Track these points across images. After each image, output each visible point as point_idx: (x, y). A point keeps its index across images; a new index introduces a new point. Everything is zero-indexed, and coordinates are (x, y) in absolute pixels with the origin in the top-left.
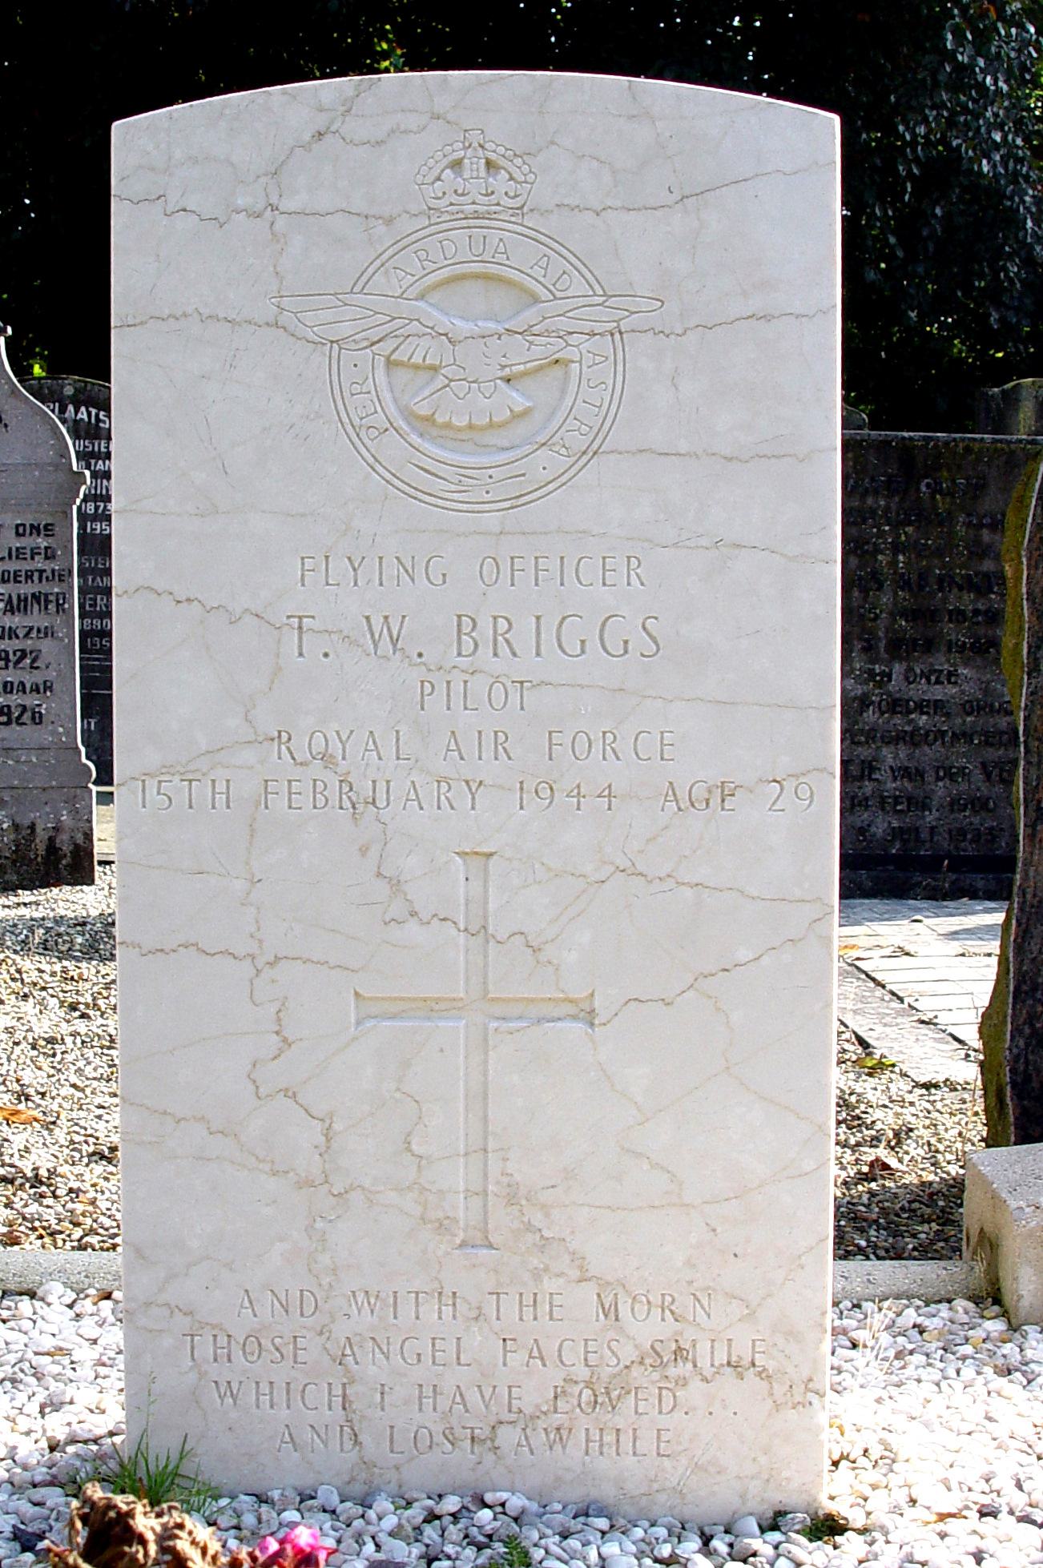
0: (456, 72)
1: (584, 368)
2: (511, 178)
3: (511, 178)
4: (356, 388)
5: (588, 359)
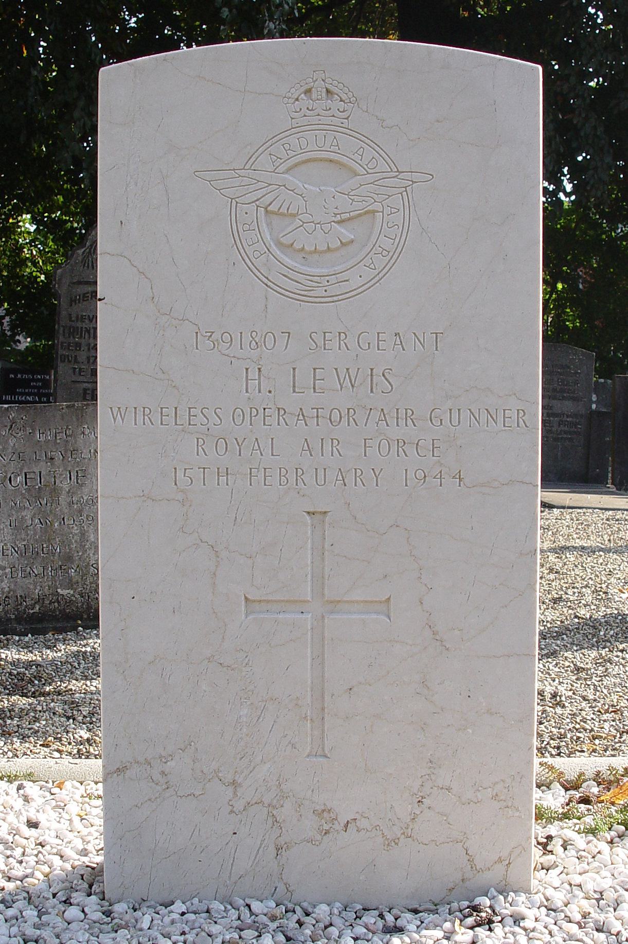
0: (589, 496)
1: (385, 215)
3: (341, 101)
5: (387, 210)
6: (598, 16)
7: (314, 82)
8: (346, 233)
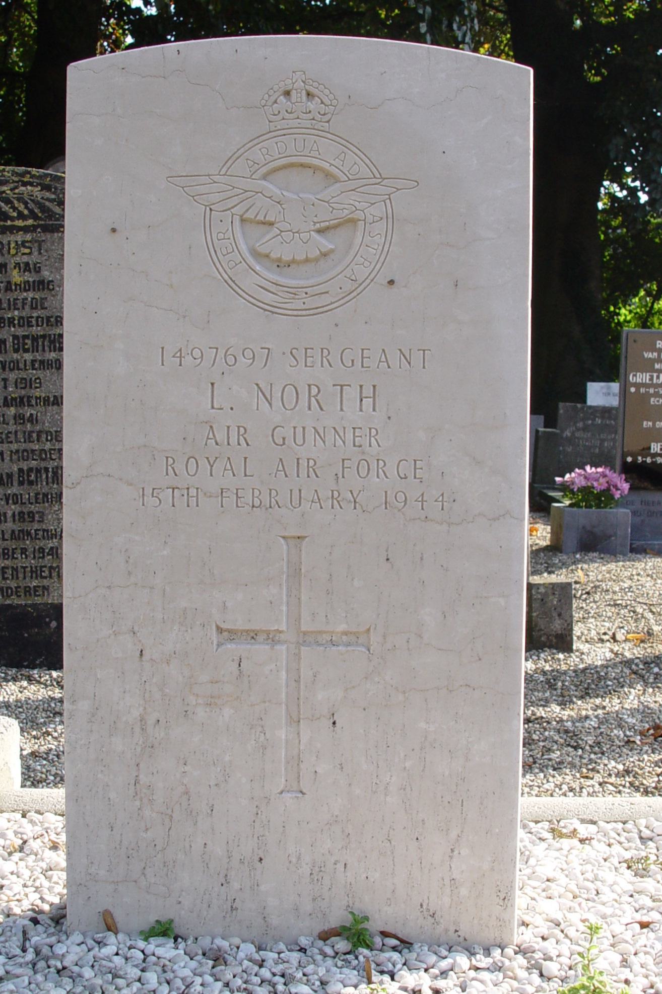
2: (322, 103)
3: (322, 103)
4: (221, 236)
6: (596, 75)
7: (294, 84)
8: (325, 243)
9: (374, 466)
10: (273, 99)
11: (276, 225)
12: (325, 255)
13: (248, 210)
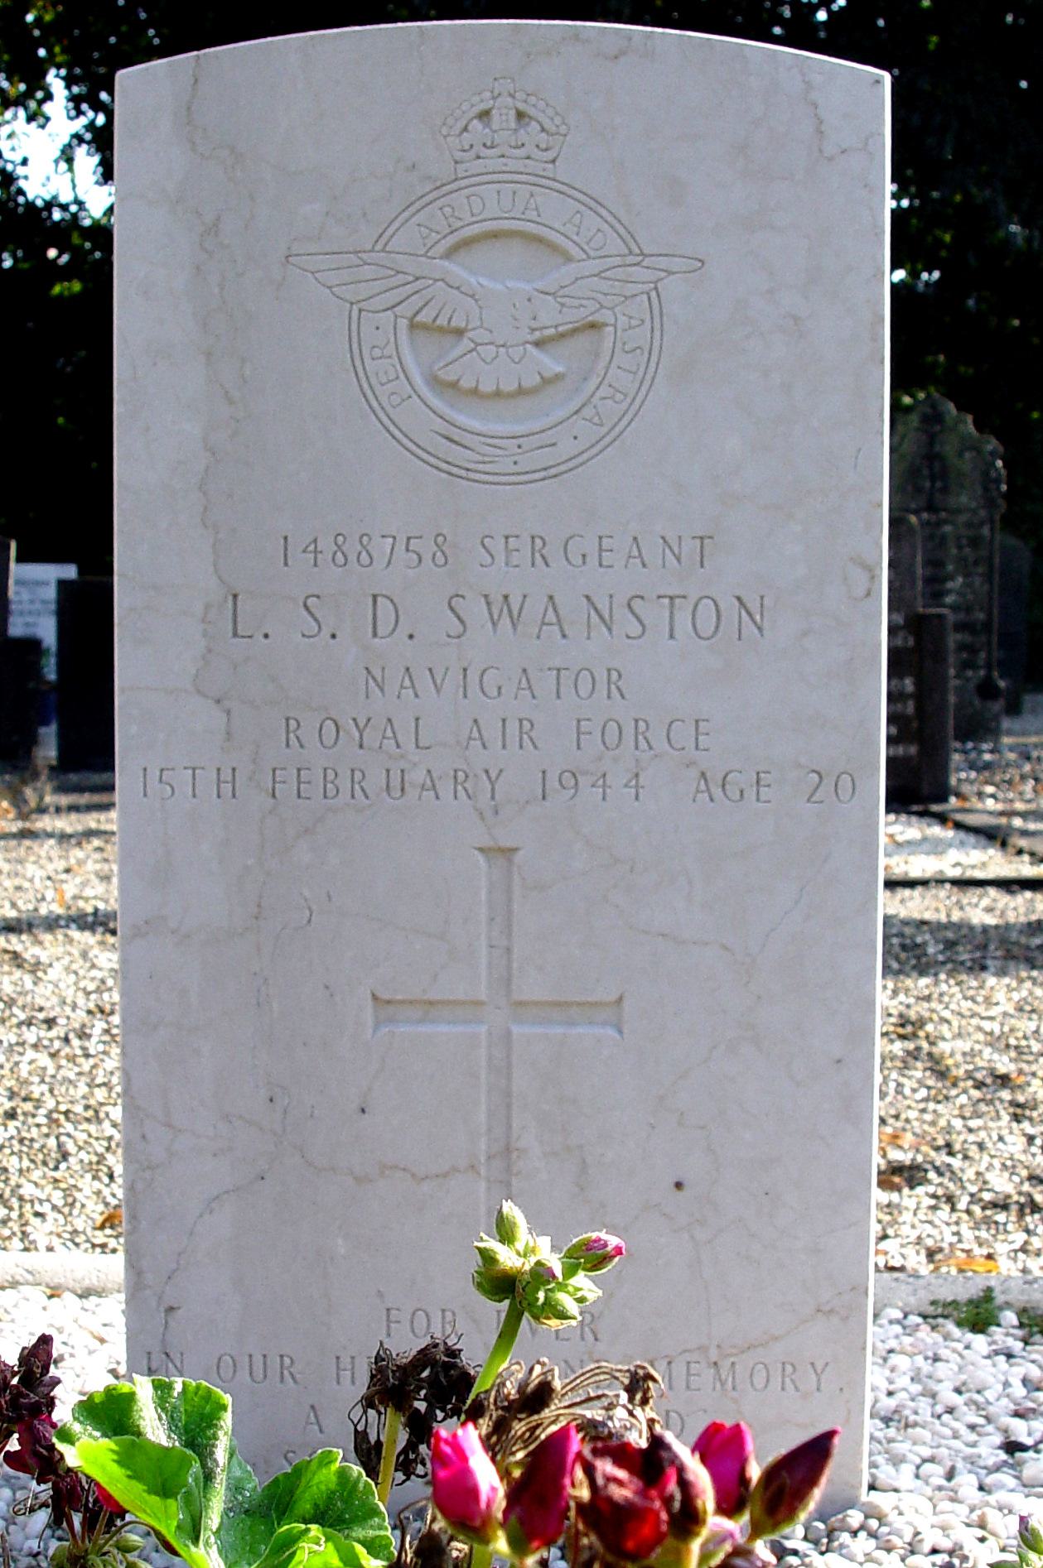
2: (543, 130)
4: (377, 352)
7: (494, 98)
8: (550, 363)
9: (629, 730)
10: (461, 125)
11: (470, 334)
12: (546, 382)
13: (421, 309)
